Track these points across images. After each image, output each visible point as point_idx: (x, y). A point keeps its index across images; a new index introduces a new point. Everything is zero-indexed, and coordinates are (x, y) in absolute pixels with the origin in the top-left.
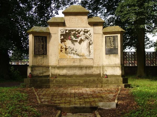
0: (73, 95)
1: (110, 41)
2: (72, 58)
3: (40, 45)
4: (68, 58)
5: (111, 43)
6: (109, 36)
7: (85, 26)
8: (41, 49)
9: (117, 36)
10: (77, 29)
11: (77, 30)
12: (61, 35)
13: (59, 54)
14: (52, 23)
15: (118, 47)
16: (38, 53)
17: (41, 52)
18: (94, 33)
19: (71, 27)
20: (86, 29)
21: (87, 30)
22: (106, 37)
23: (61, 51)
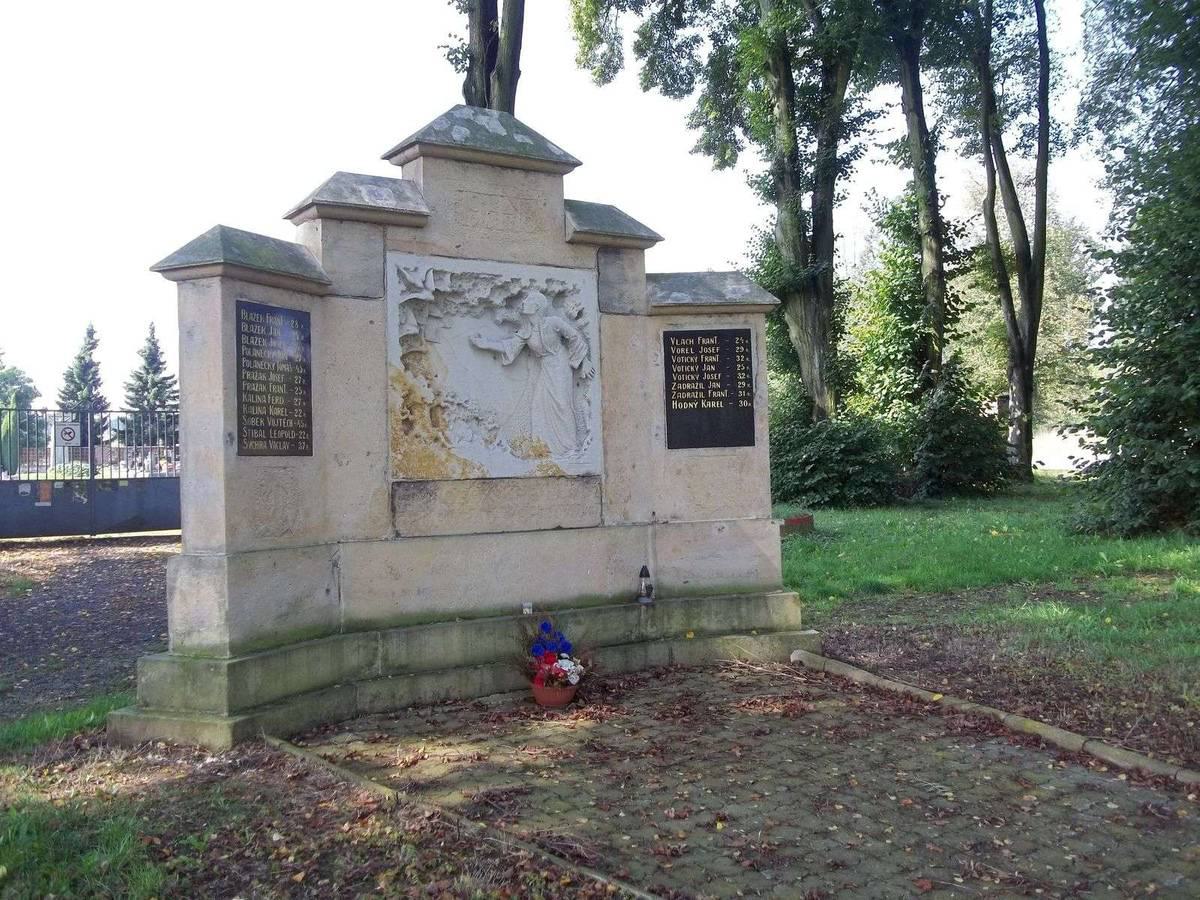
0: (916, 699)
1: (701, 364)
2: (477, 474)
3: (273, 377)
4: (455, 476)
5: (707, 377)
6: (693, 334)
7: (549, 255)
8: (279, 411)
9: (746, 334)
10: (507, 272)
11: (506, 278)
12: (403, 305)
13: (395, 445)
14: (384, 217)
15: (751, 399)
16: (261, 445)
17: (281, 434)
18: (604, 308)
19: (465, 254)
20: (556, 278)
21: (563, 283)
22: (667, 335)
23: (408, 424)
